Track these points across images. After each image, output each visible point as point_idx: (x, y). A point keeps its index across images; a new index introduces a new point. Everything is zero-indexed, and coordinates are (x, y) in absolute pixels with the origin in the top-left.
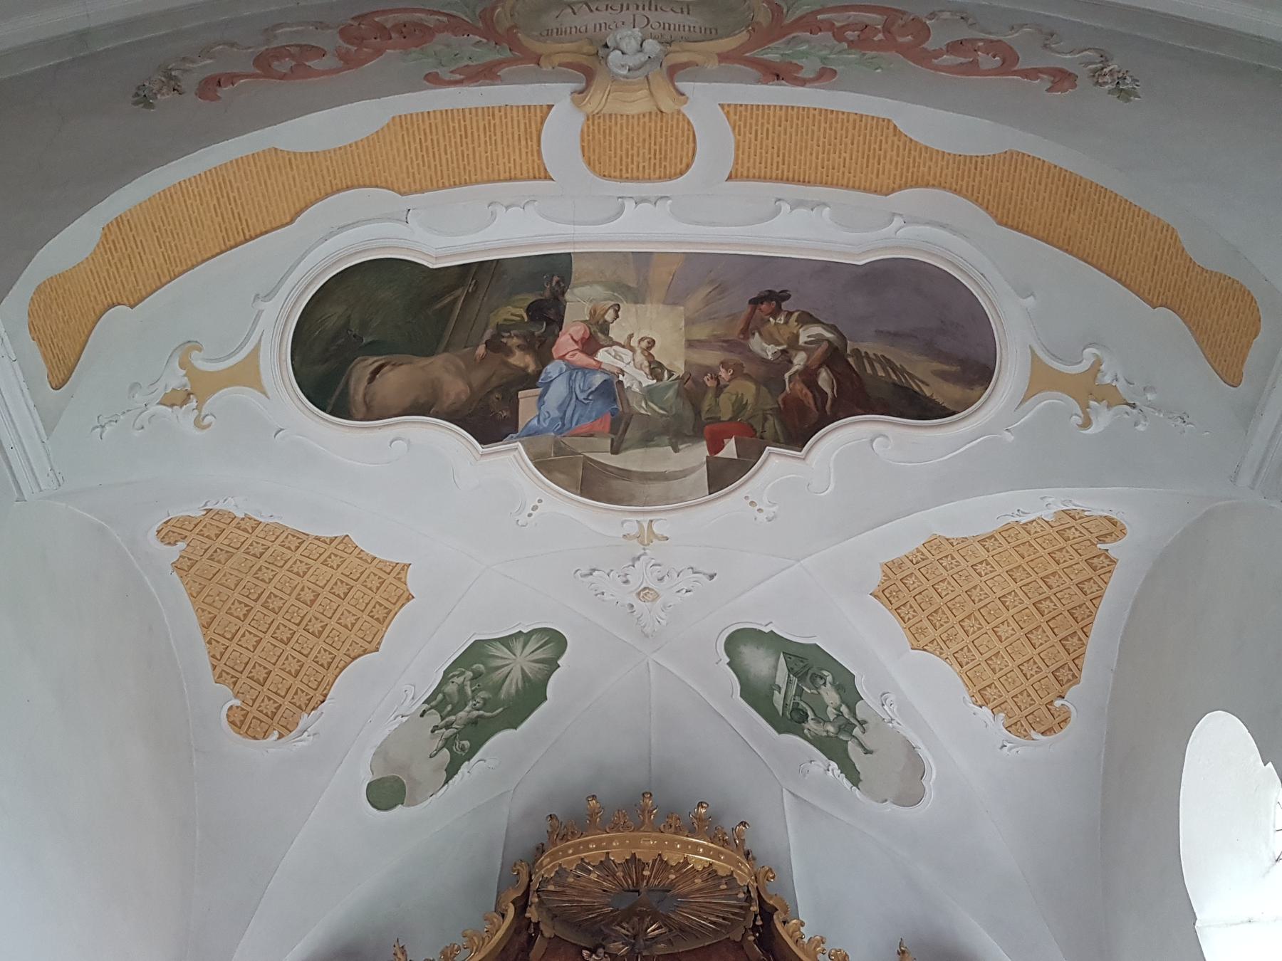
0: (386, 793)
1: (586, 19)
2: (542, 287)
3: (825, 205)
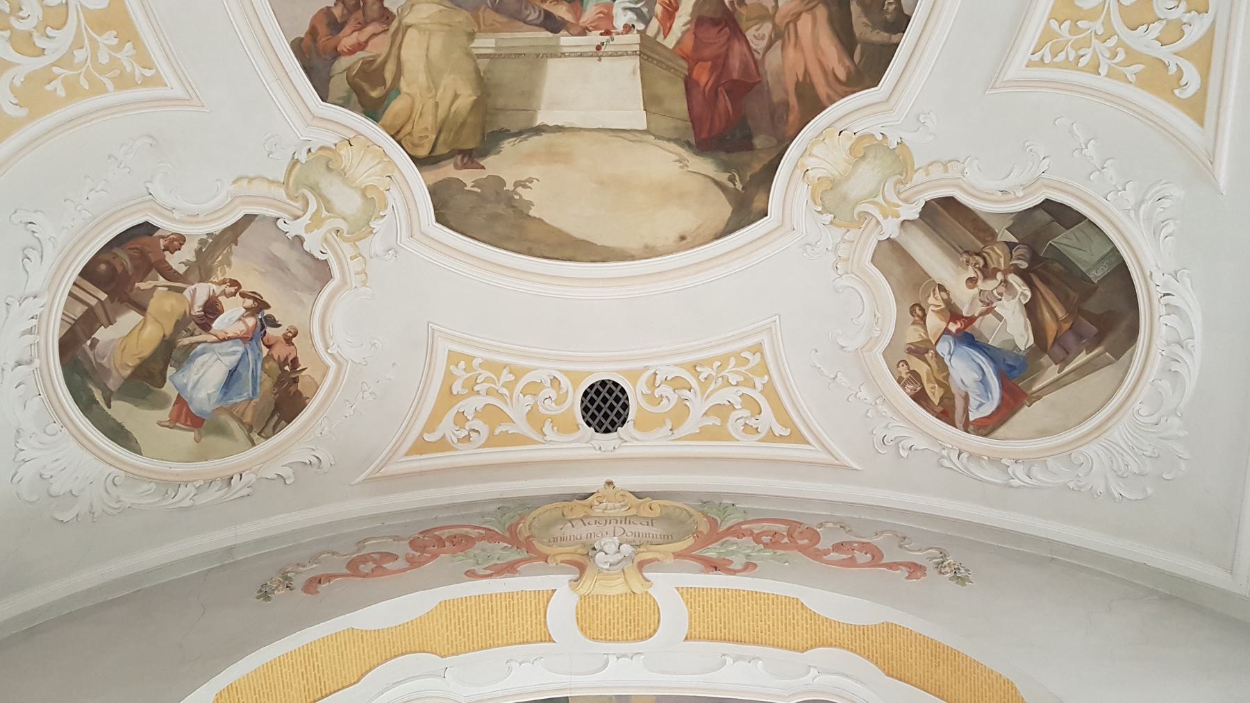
1: (581, 531)
3: (759, 659)
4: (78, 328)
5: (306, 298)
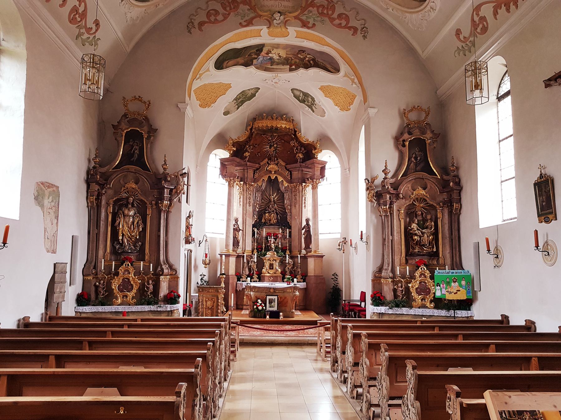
0: (226, 113)
2: (259, 48)
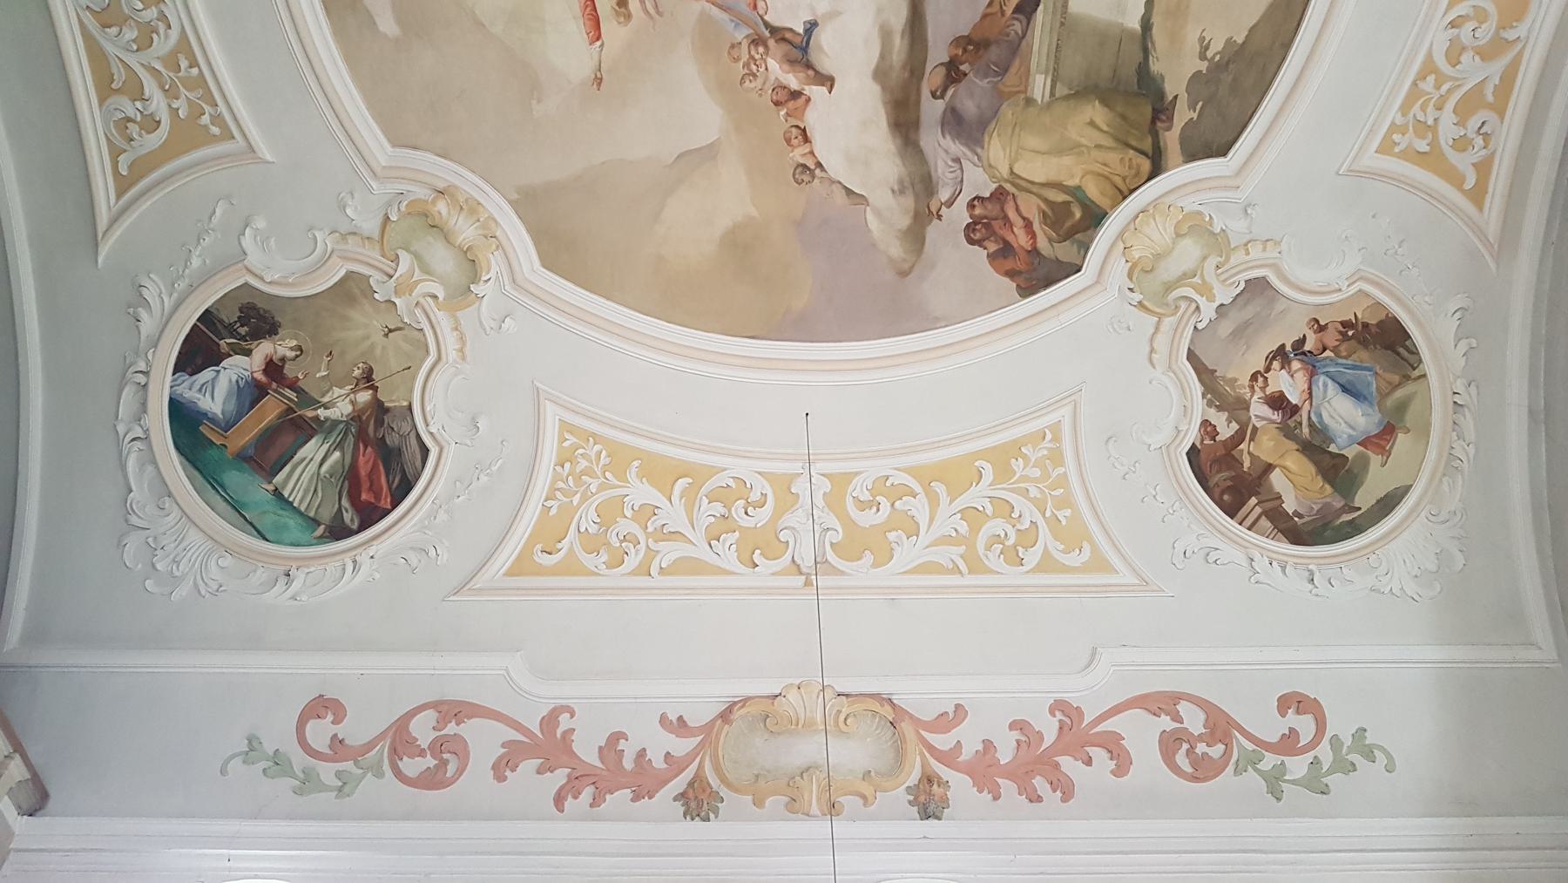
4: (1283, 526)
5: (1281, 305)
